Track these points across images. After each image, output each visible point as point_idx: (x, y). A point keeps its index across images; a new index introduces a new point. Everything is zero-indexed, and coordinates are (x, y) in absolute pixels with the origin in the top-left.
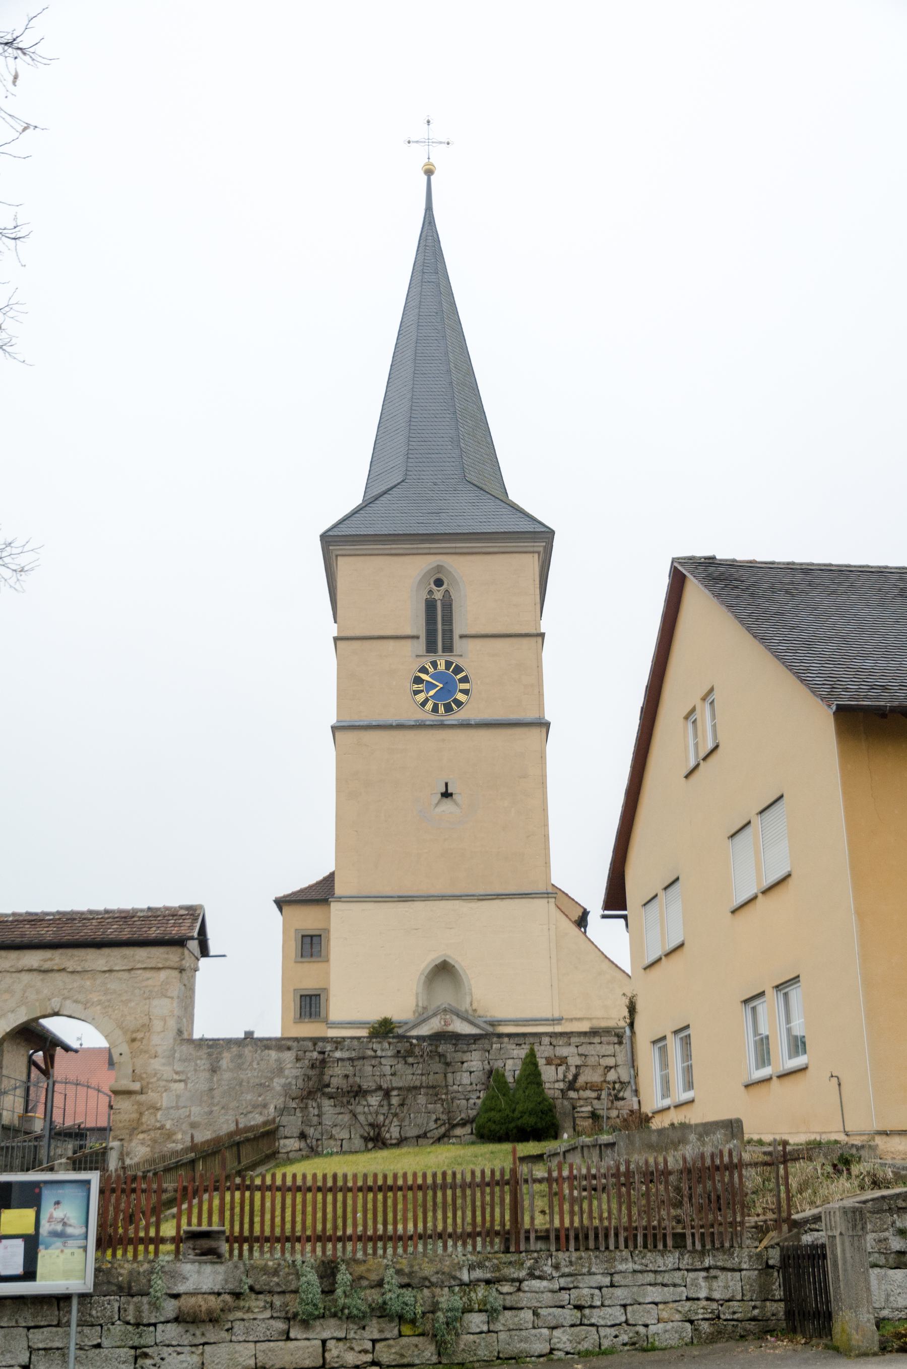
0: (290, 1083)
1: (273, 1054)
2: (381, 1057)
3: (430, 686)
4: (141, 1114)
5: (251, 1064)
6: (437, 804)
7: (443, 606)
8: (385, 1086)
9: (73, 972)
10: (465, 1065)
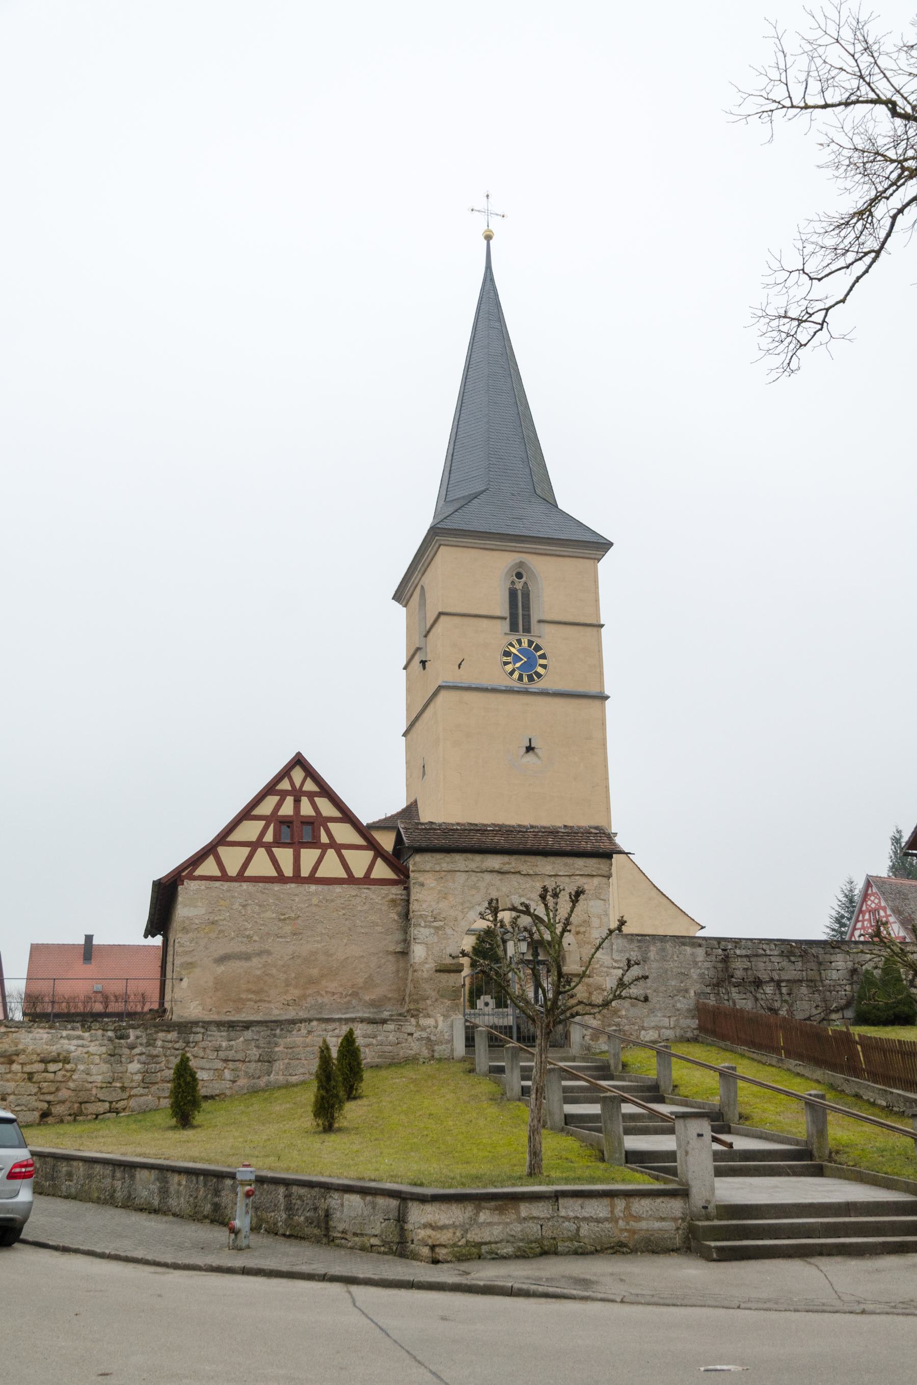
0: (703, 973)
1: (688, 949)
2: (770, 955)
3: (517, 659)
4: (591, 994)
6: (523, 756)
7: (523, 594)
8: (776, 977)
9: (525, 875)
10: (833, 964)
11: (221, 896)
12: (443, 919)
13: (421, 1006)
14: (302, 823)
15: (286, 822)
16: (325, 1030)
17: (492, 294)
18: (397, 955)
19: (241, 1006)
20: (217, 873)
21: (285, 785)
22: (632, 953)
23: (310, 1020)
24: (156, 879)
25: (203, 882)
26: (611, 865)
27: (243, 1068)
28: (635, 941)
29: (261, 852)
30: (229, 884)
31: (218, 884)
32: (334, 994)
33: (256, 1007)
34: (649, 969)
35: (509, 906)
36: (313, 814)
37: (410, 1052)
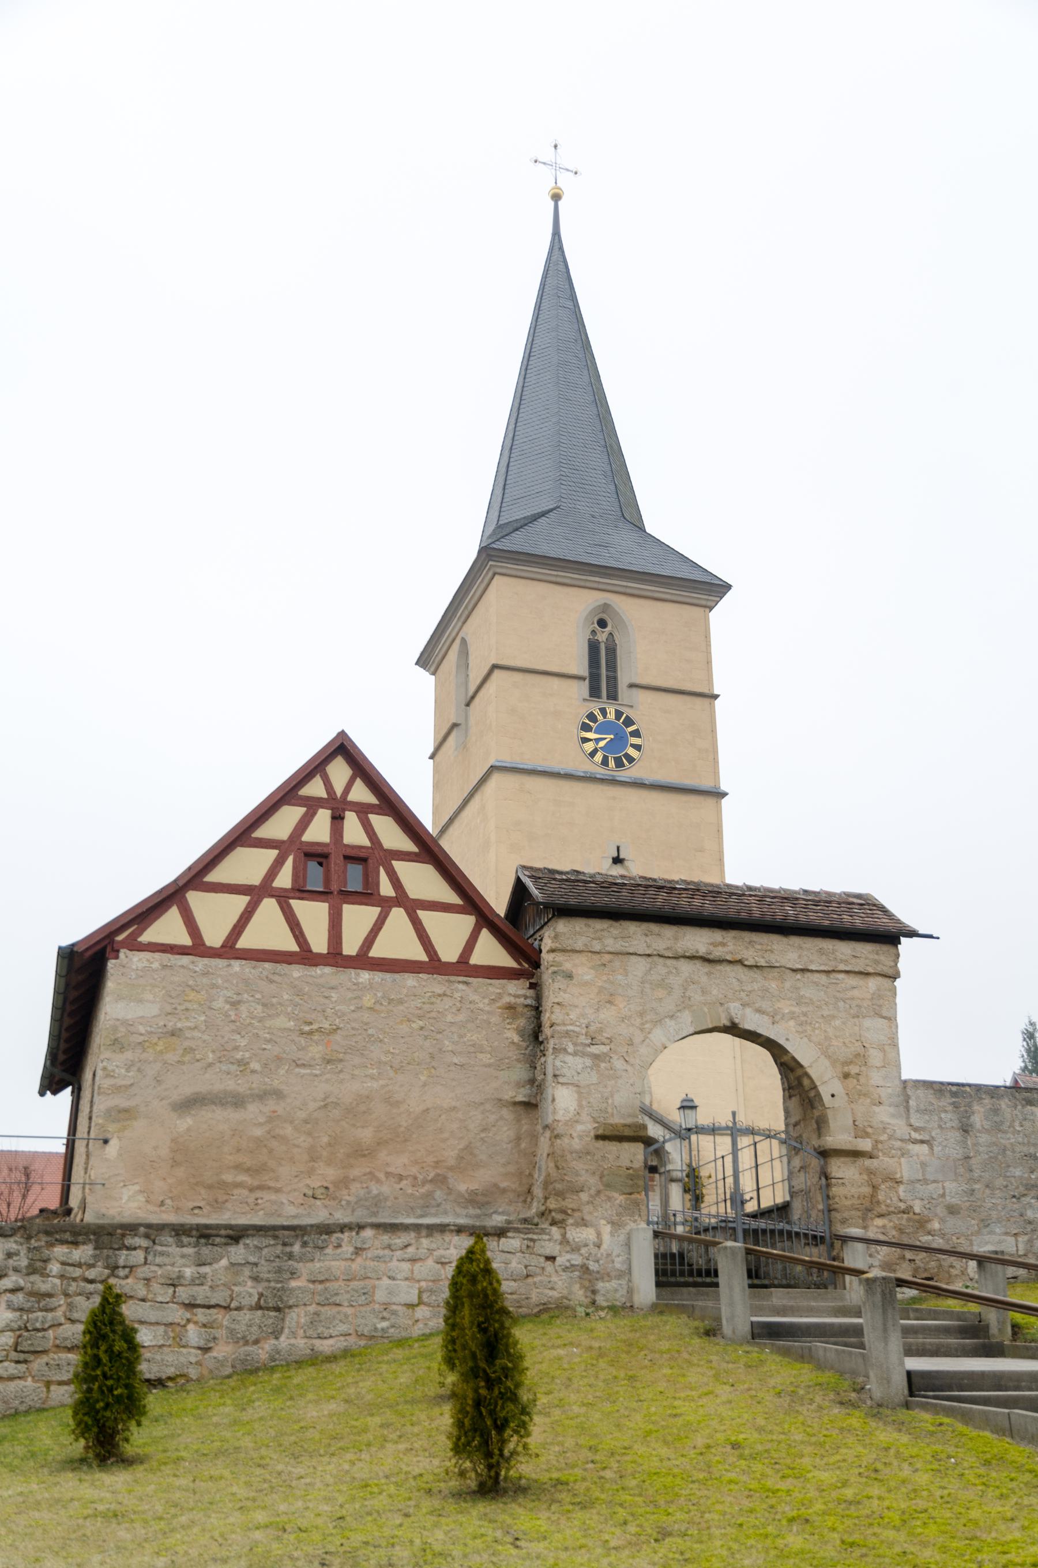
4: (875, 1188)
5: (1011, 1126)
9: (750, 967)
11: (191, 983)
12: (607, 1041)
13: (569, 1203)
14: (347, 858)
15: (317, 855)
16: (389, 1247)
17: (562, 267)
18: (519, 1108)
19: (222, 1198)
20: (185, 939)
21: (315, 788)
22: (943, 1115)
23: (361, 1227)
24: (67, 941)
25: (157, 955)
26: (898, 956)
27: (225, 1323)
28: (948, 1095)
29: (269, 906)
30: (206, 960)
31: (185, 960)
32: (401, 1178)
33: (251, 1200)
34: (974, 1145)
35: (725, 1022)
36: (367, 842)
37: (551, 1293)
